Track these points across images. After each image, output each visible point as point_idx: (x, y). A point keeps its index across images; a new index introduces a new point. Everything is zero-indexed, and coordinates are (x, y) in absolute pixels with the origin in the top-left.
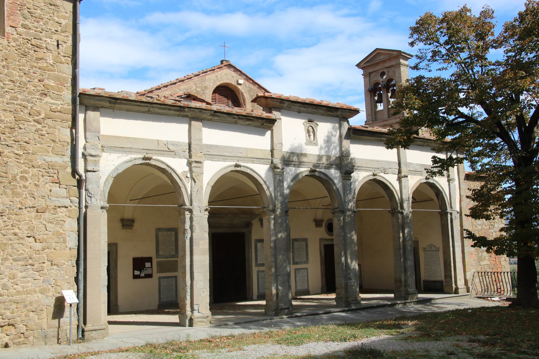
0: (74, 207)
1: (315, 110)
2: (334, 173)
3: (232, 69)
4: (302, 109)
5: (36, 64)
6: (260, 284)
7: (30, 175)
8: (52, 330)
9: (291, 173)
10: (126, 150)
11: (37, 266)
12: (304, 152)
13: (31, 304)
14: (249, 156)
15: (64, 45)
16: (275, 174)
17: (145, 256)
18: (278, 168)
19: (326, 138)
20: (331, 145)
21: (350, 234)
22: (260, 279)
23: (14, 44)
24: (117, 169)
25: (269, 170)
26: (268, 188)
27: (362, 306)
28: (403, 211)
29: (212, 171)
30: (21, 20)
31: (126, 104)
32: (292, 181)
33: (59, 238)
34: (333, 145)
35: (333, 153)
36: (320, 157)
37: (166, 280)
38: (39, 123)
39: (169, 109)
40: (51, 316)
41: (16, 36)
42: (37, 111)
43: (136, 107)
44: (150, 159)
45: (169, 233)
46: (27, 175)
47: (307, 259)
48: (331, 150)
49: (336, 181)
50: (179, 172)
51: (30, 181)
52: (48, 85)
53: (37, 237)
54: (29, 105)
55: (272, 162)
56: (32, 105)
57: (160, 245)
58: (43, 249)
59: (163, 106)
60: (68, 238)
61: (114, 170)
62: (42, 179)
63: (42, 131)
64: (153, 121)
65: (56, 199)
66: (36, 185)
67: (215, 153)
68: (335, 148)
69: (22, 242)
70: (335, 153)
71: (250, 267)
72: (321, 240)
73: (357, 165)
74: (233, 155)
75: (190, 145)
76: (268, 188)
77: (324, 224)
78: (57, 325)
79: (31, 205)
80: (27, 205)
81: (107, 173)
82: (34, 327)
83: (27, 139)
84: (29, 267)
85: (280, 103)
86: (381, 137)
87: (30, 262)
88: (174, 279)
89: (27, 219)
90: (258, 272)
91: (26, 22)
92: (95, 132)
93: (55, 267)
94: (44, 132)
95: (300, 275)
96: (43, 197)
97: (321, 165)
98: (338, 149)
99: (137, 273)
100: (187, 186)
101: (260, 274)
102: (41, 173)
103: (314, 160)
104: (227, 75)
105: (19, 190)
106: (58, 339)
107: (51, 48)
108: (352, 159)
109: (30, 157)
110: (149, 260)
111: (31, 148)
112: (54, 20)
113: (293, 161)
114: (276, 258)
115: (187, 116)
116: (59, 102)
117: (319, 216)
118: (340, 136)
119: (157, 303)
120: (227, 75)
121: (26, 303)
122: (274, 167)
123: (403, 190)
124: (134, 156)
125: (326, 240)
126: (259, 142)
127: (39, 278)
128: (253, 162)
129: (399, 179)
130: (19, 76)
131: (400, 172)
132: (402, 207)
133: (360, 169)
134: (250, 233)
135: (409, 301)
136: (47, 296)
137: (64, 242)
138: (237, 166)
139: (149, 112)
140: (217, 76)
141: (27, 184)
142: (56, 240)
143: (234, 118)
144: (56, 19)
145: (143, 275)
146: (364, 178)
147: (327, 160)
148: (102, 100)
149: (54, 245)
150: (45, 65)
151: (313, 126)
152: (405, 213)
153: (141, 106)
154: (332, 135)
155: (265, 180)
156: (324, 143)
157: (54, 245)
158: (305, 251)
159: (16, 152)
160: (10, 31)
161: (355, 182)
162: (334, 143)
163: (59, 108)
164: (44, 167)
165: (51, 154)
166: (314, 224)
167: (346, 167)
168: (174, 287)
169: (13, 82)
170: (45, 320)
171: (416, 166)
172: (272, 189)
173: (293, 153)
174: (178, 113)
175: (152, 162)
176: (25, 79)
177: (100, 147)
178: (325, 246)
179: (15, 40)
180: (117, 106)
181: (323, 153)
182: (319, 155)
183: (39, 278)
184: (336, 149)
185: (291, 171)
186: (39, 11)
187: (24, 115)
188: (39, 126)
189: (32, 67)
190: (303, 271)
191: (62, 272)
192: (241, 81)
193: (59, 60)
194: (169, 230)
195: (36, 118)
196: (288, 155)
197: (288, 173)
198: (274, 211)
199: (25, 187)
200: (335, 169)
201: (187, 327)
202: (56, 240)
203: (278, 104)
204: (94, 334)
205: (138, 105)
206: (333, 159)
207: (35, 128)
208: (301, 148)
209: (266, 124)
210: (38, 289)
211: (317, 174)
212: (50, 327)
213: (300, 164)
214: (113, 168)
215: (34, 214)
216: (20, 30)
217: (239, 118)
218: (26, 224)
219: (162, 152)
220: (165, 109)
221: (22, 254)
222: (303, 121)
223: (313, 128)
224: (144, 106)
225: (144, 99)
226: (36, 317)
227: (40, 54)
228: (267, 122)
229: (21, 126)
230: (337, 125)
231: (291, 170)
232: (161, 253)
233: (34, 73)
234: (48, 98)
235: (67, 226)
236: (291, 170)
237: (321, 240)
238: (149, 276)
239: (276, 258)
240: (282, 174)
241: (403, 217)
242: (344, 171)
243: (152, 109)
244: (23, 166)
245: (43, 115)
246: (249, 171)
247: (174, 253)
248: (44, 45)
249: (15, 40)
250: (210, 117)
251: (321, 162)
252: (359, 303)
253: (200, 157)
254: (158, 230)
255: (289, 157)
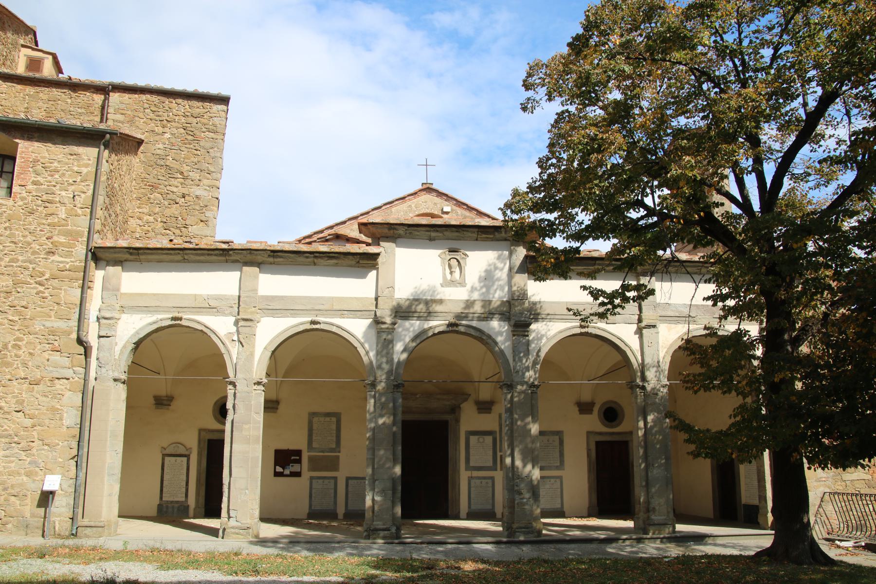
0: (76, 379)
1: (457, 234)
2: (497, 327)
3: (435, 194)
4: (433, 234)
5: (44, 221)
6: (472, 496)
7: (24, 342)
8: (36, 519)
9: (411, 329)
10: (151, 309)
11: (24, 444)
12: (438, 297)
13: (12, 486)
14: (335, 308)
15: (83, 195)
16: (379, 332)
17: (292, 447)
18: (384, 323)
19: (483, 274)
20: (493, 285)
21: (523, 420)
22: (472, 489)
23: (21, 203)
24: (137, 333)
25: (370, 326)
26: (367, 353)
27: (543, 538)
28: (646, 384)
29: (270, 331)
30: (33, 177)
31: (152, 254)
32: (413, 340)
33: (54, 414)
34: (497, 283)
35: (497, 295)
36: (469, 304)
37: (320, 481)
38: (40, 284)
39: (208, 255)
40: (36, 503)
41: (25, 195)
42: (40, 272)
43: (165, 256)
44: (181, 319)
45: (328, 419)
46: (20, 343)
47: (562, 462)
48: (492, 291)
49: (499, 339)
50: (222, 333)
51: (24, 349)
52: (57, 242)
53: (27, 412)
54: (31, 266)
55: (376, 315)
56: (34, 266)
57: (314, 435)
58: (33, 426)
59: (199, 252)
60: (65, 415)
61: (134, 335)
62: (39, 347)
63: (44, 293)
64: (191, 271)
65: (55, 369)
66: (31, 354)
67: (277, 307)
68: (501, 288)
69: (8, 416)
70: (499, 295)
71: (457, 471)
72: (589, 433)
73: (546, 312)
74: (308, 308)
75: (239, 297)
76: (367, 353)
77: (596, 409)
78: (43, 514)
79: (23, 376)
80: (17, 377)
81: (125, 339)
82: (14, 514)
83: (24, 303)
84: (13, 445)
85: (389, 229)
86: (595, 264)
87: (16, 439)
88: (333, 481)
89: (16, 391)
90: (470, 479)
91: (39, 178)
92: (113, 290)
93: (46, 447)
94: (46, 295)
95: (547, 486)
96: (38, 367)
97: (471, 315)
98: (506, 289)
99: (279, 469)
100: (233, 353)
101: (473, 482)
102: (38, 341)
103: (458, 309)
104: (426, 202)
105: (9, 359)
106: (44, 531)
107: (66, 201)
108: (535, 304)
109: (26, 323)
110: (299, 453)
111: (29, 313)
112: (72, 170)
113: (415, 312)
114: (374, 454)
115: (236, 261)
116: (68, 260)
117: (586, 397)
118: (510, 269)
119: (307, 511)
120: (426, 202)
121: (6, 486)
122: (377, 321)
123: (646, 349)
124: (160, 316)
125: (601, 434)
126: (357, 288)
127: (25, 458)
128: (342, 316)
129: (639, 332)
130: (23, 236)
131: (640, 320)
132: (644, 378)
133: (551, 317)
134: (457, 421)
135: (648, 536)
136: (34, 481)
137: (61, 419)
138: (313, 322)
139: (184, 260)
140: (410, 206)
141: (21, 352)
142: (51, 416)
143: (307, 257)
144: (76, 169)
145: (287, 472)
146: (561, 332)
147: (483, 307)
148: (119, 253)
149: (47, 421)
150: (56, 220)
151: (458, 258)
152: (649, 388)
153: (171, 254)
154: (496, 268)
155: (362, 341)
156: (480, 281)
157: (47, 421)
158: (557, 450)
159: (11, 318)
160: (19, 191)
161: (539, 339)
162: (499, 279)
163: (68, 266)
164: (43, 333)
165: (53, 318)
166: (576, 409)
167: (520, 316)
168: (333, 491)
169: (15, 243)
170: (28, 507)
171: (682, 309)
172: (372, 354)
173: (417, 300)
174: (224, 258)
175: (183, 323)
176: (29, 239)
177: (118, 308)
178: (598, 443)
179: (23, 199)
180: (142, 257)
181: (476, 296)
182: (467, 301)
183: (25, 458)
184: (503, 290)
185: (410, 328)
186: (56, 164)
187: (24, 276)
188: (41, 288)
189: (39, 224)
190: (552, 480)
191: (54, 454)
192: (447, 209)
193: (74, 213)
194: (328, 415)
195: (38, 279)
196: (408, 302)
197: (408, 330)
198: (373, 385)
199: (16, 356)
200: (500, 320)
201: (220, 539)
202: (51, 416)
203: (386, 231)
204: (88, 531)
205: (167, 254)
206: (496, 304)
207: (35, 291)
208: (434, 291)
209: (368, 261)
210: (23, 471)
211: (462, 329)
212: (33, 515)
213: (429, 315)
214: (133, 331)
215: (26, 386)
216: (30, 187)
217: (315, 257)
218: (13, 397)
219: (200, 309)
220: (203, 255)
221: (6, 430)
222: (440, 251)
223: (458, 261)
224: (175, 254)
225: (304, 248)
226: (18, 502)
227: (52, 208)
228: (363, 259)
229: (19, 290)
230: (506, 253)
231: (412, 325)
232: (315, 445)
233: (41, 231)
234: (57, 256)
235: (65, 400)
236: (412, 325)
237: (589, 433)
238: (298, 474)
239: (374, 454)
240: (391, 330)
241: (646, 395)
242: (512, 322)
243: (186, 257)
244: (17, 333)
245: (47, 276)
246: (334, 329)
247: (334, 446)
248: (57, 199)
249: (23, 199)
250: (271, 260)
251: (471, 311)
252: (539, 532)
253: (252, 313)
254: (313, 415)
255: (410, 306)
